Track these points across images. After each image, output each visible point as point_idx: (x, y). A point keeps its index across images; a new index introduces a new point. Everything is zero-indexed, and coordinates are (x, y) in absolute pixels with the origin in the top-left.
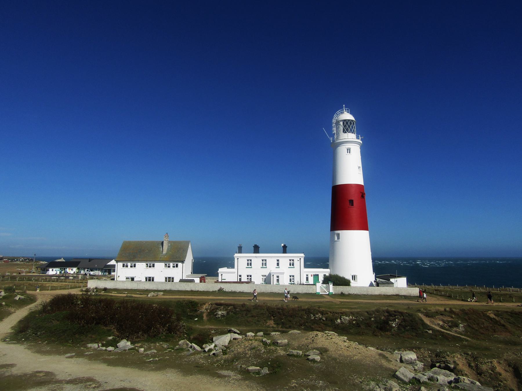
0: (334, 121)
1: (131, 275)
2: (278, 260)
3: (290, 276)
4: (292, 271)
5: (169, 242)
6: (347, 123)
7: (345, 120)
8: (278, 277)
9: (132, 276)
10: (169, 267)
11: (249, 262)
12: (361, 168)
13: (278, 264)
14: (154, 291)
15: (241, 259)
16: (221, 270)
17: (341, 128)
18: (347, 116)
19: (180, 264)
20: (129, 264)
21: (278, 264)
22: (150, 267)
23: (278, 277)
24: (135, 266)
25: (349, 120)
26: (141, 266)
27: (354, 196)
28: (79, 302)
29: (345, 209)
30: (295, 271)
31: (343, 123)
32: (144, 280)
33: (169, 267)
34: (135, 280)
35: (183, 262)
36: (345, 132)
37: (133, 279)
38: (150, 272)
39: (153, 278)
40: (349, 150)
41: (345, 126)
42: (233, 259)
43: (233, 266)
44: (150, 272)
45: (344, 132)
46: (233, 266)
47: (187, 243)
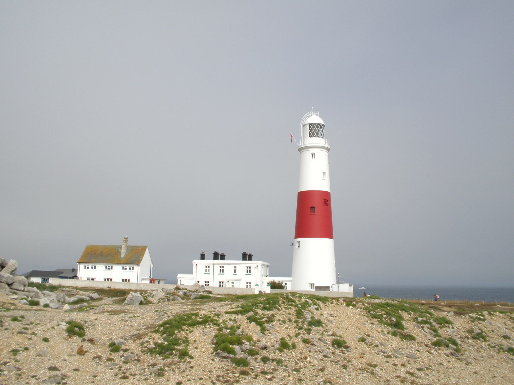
0: (302, 125)
1: (91, 277)
2: (235, 267)
3: (247, 283)
4: (249, 279)
5: (128, 247)
6: (313, 127)
7: (311, 124)
8: (233, 283)
9: (93, 277)
10: (126, 269)
11: (222, 269)
12: (327, 176)
13: (235, 271)
14: (68, 287)
15: (200, 266)
16: (179, 276)
17: (308, 131)
18: (315, 119)
19: (136, 267)
20: (128, 268)
21: (235, 271)
22: (109, 269)
23: (233, 283)
24: (95, 268)
25: (319, 124)
26: (101, 267)
27: (317, 203)
28: (384, 316)
29: (313, 215)
30: (252, 278)
31: (310, 127)
32: (121, 281)
33: (126, 269)
34: (130, 281)
35: (138, 264)
36: (311, 137)
37: (93, 279)
38: (108, 274)
39: (129, 280)
40: (313, 155)
41: (311, 130)
42: (192, 265)
43: (191, 273)
44: (108, 274)
45: (310, 136)
46: (191, 273)
47: (144, 249)
